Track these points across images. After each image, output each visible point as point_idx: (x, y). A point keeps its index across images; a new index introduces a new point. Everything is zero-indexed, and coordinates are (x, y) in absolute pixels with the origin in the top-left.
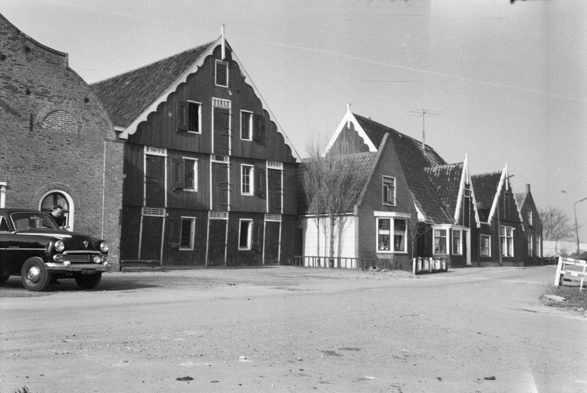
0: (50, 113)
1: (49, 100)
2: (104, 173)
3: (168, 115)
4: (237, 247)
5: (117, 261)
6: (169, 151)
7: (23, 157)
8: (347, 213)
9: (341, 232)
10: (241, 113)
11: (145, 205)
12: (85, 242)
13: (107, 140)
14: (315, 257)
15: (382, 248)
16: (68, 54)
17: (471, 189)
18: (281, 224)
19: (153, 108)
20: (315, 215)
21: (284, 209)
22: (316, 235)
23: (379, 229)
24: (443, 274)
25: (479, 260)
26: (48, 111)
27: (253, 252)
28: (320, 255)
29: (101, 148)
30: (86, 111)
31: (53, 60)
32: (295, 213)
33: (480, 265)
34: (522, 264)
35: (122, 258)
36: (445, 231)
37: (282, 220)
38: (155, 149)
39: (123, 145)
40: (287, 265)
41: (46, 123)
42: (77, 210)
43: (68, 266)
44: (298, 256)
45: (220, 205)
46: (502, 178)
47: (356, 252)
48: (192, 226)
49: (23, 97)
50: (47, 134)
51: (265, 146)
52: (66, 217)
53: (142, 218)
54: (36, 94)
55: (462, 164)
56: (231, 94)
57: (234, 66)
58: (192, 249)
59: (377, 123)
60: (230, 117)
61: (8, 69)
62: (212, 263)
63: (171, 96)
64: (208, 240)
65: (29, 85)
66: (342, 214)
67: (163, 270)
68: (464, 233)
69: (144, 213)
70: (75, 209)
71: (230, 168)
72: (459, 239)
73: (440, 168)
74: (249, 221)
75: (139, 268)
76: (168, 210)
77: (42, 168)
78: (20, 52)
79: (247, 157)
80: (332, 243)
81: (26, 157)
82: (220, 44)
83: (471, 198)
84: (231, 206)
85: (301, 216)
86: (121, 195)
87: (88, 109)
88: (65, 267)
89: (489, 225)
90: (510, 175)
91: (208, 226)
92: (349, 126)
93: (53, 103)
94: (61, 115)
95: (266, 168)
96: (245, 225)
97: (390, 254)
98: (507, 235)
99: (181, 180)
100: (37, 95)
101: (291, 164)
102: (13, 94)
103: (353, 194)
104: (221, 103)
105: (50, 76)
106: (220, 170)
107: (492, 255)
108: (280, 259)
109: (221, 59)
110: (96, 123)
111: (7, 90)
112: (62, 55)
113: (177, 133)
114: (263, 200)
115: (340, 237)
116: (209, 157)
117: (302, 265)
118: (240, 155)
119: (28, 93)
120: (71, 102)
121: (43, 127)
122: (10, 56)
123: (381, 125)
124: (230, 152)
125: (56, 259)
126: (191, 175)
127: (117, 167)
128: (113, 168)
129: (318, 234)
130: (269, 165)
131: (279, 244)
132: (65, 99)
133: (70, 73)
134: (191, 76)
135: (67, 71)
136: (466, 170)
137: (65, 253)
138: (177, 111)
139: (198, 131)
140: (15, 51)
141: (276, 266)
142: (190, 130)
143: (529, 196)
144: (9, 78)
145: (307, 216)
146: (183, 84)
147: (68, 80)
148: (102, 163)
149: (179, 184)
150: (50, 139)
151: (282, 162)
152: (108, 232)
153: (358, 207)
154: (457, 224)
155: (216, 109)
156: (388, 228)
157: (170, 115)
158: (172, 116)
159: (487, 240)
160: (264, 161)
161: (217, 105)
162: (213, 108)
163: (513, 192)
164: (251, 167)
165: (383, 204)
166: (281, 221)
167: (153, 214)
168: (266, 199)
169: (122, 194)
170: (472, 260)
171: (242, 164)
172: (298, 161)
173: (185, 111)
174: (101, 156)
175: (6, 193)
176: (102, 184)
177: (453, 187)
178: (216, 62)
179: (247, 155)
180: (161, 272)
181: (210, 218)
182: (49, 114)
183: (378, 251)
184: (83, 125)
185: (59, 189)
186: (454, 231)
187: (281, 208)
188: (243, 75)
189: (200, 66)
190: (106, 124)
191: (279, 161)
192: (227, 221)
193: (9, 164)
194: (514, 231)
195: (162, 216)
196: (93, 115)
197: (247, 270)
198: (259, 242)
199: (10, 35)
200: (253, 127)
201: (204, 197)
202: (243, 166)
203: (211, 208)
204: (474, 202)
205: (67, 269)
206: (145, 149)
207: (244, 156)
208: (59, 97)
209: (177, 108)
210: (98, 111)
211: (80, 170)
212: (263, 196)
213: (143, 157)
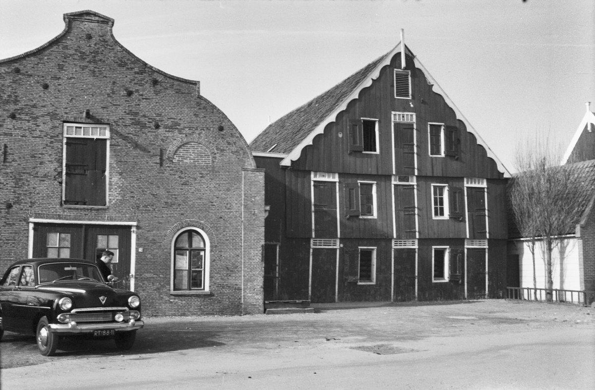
0: (181, 146)
2: (243, 206)
3: (337, 136)
5: (261, 302)
6: (341, 175)
7: (153, 195)
10: (429, 125)
11: (313, 236)
12: (101, 298)
13: (245, 170)
14: (531, 289)
16: (199, 82)
18: (487, 250)
19: (320, 129)
20: (529, 239)
21: (489, 233)
22: (533, 261)
26: (180, 144)
28: (537, 287)
29: (238, 179)
30: (220, 140)
31: (183, 90)
35: (265, 298)
37: (488, 246)
38: (323, 174)
40: (499, 298)
43: (73, 327)
44: (511, 288)
45: (407, 231)
48: (373, 258)
49: (153, 132)
51: (461, 161)
53: (311, 251)
54: (166, 127)
56: (412, 106)
57: (418, 74)
58: (374, 283)
60: (415, 132)
61: (136, 105)
62: (399, 298)
63: (340, 116)
64: (393, 272)
65: (158, 118)
67: (317, 311)
69: (314, 245)
70: (211, 247)
71: (417, 190)
74: (446, 249)
75: (288, 309)
77: (174, 204)
78: (147, 85)
79: (439, 175)
80: (550, 272)
81: (156, 195)
82: (400, 51)
84: (419, 232)
85: (515, 239)
86: (263, 229)
88: (69, 329)
91: (393, 256)
93: (184, 135)
94: (193, 147)
96: (440, 254)
100: (167, 128)
101: (498, 180)
102: (141, 130)
104: (403, 117)
106: (404, 194)
109: (400, 67)
111: (135, 127)
112: (193, 84)
114: (462, 223)
115: (562, 264)
116: (464, 180)
117: (520, 299)
118: (429, 174)
119: (157, 127)
120: (204, 132)
121: (174, 161)
122: (137, 91)
125: (60, 319)
128: (253, 200)
129: (534, 262)
130: (467, 183)
131: (485, 273)
133: (202, 102)
135: (198, 100)
137: (73, 311)
138: (348, 131)
139: (375, 151)
140: (141, 85)
141: (483, 300)
142: (365, 150)
144: (136, 114)
145: (522, 239)
146: (355, 100)
148: (240, 196)
150: (182, 174)
152: (249, 270)
153: (581, 227)
155: (397, 125)
157: (340, 136)
160: (461, 179)
161: (398, 120)
162: (393, 124)
164: (444, 187)
166: (487, 247)
167: (324, 245)
168: (465, 222)
169: (264, 228)
172: (506, 176)
174: (239, 188)
175: (137, 233)
176: (241, 218)
178: (395, 72)
179: (438, 172)
181: (394, 247)
182: (180, 147)
184: (217, 155)
187: (486, 232)
189: (375, 78)
190: (244, 153)
191: (481, 177)
192: (417, 250)
193: (138, 202)
195: (335, 247)
196: (229, 144)
199: (136, 70)
200: (445, 141)
201: (385, 224)
202: (434, 186)
203: (395, 236)
205: (71, 331)
206: (312, 175)
207: (435, 175)
209: (348, 127)
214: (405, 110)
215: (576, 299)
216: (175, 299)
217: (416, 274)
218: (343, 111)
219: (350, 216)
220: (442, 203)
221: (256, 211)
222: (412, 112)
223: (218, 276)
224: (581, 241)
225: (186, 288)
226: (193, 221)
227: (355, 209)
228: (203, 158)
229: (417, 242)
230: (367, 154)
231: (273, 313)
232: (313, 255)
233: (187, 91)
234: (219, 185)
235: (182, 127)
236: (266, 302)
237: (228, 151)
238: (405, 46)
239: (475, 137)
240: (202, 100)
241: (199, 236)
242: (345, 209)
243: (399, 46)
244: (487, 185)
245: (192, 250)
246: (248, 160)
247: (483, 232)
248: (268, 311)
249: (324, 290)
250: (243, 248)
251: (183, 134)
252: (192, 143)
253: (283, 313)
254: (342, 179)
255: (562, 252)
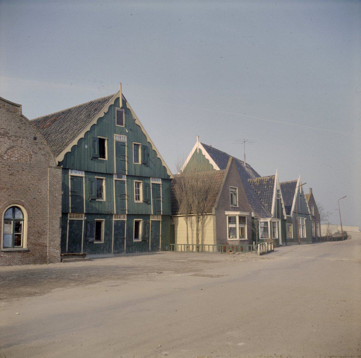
1: (9, 139)
4: (133, 239)
5: (59, 254)
8: (207, 213)
9: (203, 227)
10: (133, 144)
13: (50, 167)
15: (231, 237)
16: (21, 105)
17: (280, 193)
18: (161, 222)
19: (75, 142)
20: (184, 215)
21: (163, 212)
22: (184, 228)
23: (228, 224)
24: (272, 253)
25: (286, 241)
26: (8, 147)
27: (143, 242)
30: (35, 146)
32: (170, 214)
33: (287, 244)
34: (311, 242)
36: (267, 222)
37: (162, 219)
39: (61, 170)
41: (6, 155)
42: (29, 219)
46: (297, 185)
47: (214, 240)
50: (8, 164)
52: (21, 224)
53: (68, 221)
55: (274, 177)
56: (127, 131)
57: (128, 111)
59: (216, 149)
62: (116, 251)
64: (113, 235)
66: (205, 214)
67: (90, 260)
68: (278, 222)
69: (70, 218)
71: (127, 184)
72: (276, 228)
73: (259, 179)
75: (74, 259)
76: (86, 214)
77: (4, 188)
79: (138, 175)
83: (281, 199)
86: (61, 207)
87: (36, 145)
89: (291, 217)
90: (302, 184)
92: (198, 151)
94: (17, 149)
95: (150, 183)
96: (137, 223)
97: (237, 240)
98: (302, 223)
99: (94, 194)
101: (167, 179)
103: (208, 199)
105: (9, 121)
107: (293, 237)
108: (161, 246)
109: (119, 107)
110: (42, 155)
112: (17, 106)
113: (92, 159)
117: (173, 250)
118: (134, 175)
120: (24, 140)
123: (221, 151)
124: (127, 172)
126: (101, 189)
127: (58, 186)
128: (55, 187)
130: (152, 181)
132: (20, 138)
134: (100, 119)
135: (21, 118)
136: (277, 180)
143: (312, 195)
145: (178, 215)
147: (22, 124)
148: (47, 184)
149: (93, 196)
150: (10, 167)
151: (160, 178)
154: (273, 217)
156: (235, 222)
157: (86, 147)
158: (87, 148)
159: (290, 227)
162: (115, 142)
163: (304, 194)
165: (231, 206)
166: (161, 220)
170: (282, 242)
171: (135, 181)
172: (171, 177)
173: (97, 144)
174: (46, 179)
176: (47, 199)
177: (269, 192)
178: (116, 109)
180: (90, 261)
183: (228, 239)
184: (33, 156)
185: (17, 204)
186: (273, 222)
187: (161, 211)
188: (134, 118)
192: (126, 221)
194: (305, 220)
195: (82, 219)
196: (40, 149)
197: (139, 257)
198: (147, 236)
202: (136, 182)
204: (282, 202)
206: (70, 172)
207: (136, 175)
208: (16, 137)
209: (91, 142)
210: (43, 146)
211: (31, 189)
212: (149, 203)
213: (68, 177)
214: (121, 133)
215: (211, 250)
216: (4, 254)
217: (125, 237)
218: (88, 131)
219: (91, 199)
220: (139, 193)
221: (57, 194)
222: (125, 135)
223: (32, 238)
224: (215, 217)
225: (11, 246)
226: (17, 200)
227: (94, 195)
228: (24, 158)
229: (126, 216)
230: (101, 160)
231: (67, 261)
232: (69, 224)
233: (13, 111)
234: (34, 177)
235: (10, 135)
236: (62, 255)
237: (39, 154)
238: (122, 94)
239: (156, 153)
240: (23, 118)
241: (20, 211)
242: (88, 195)
243: (119, 93)
244: (162, 182)
245: (15, 220)
246: (52, 160)
247: (159, 211)
248: (64, 260)
249: (75, 247)
250: (48, 219)
251: (11, 140)
252: (17, 147)
253: (73, 262)
254: (87, 176)
255: (203, 223)
